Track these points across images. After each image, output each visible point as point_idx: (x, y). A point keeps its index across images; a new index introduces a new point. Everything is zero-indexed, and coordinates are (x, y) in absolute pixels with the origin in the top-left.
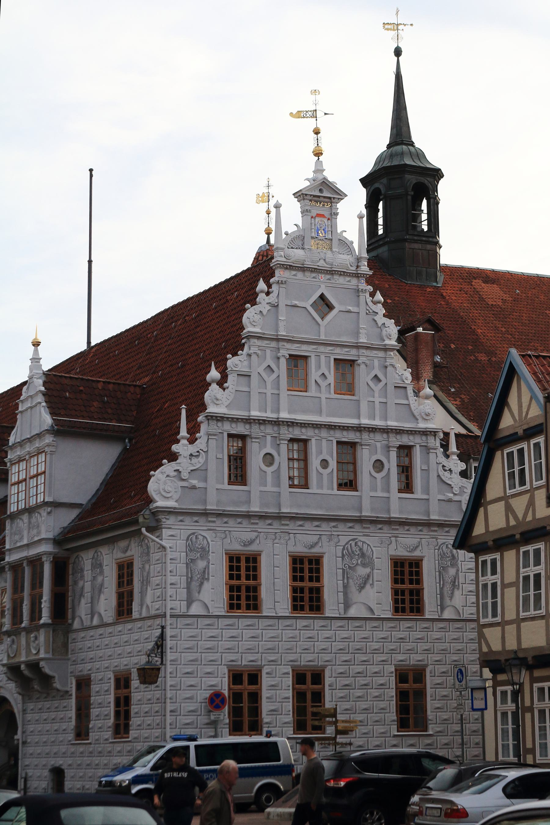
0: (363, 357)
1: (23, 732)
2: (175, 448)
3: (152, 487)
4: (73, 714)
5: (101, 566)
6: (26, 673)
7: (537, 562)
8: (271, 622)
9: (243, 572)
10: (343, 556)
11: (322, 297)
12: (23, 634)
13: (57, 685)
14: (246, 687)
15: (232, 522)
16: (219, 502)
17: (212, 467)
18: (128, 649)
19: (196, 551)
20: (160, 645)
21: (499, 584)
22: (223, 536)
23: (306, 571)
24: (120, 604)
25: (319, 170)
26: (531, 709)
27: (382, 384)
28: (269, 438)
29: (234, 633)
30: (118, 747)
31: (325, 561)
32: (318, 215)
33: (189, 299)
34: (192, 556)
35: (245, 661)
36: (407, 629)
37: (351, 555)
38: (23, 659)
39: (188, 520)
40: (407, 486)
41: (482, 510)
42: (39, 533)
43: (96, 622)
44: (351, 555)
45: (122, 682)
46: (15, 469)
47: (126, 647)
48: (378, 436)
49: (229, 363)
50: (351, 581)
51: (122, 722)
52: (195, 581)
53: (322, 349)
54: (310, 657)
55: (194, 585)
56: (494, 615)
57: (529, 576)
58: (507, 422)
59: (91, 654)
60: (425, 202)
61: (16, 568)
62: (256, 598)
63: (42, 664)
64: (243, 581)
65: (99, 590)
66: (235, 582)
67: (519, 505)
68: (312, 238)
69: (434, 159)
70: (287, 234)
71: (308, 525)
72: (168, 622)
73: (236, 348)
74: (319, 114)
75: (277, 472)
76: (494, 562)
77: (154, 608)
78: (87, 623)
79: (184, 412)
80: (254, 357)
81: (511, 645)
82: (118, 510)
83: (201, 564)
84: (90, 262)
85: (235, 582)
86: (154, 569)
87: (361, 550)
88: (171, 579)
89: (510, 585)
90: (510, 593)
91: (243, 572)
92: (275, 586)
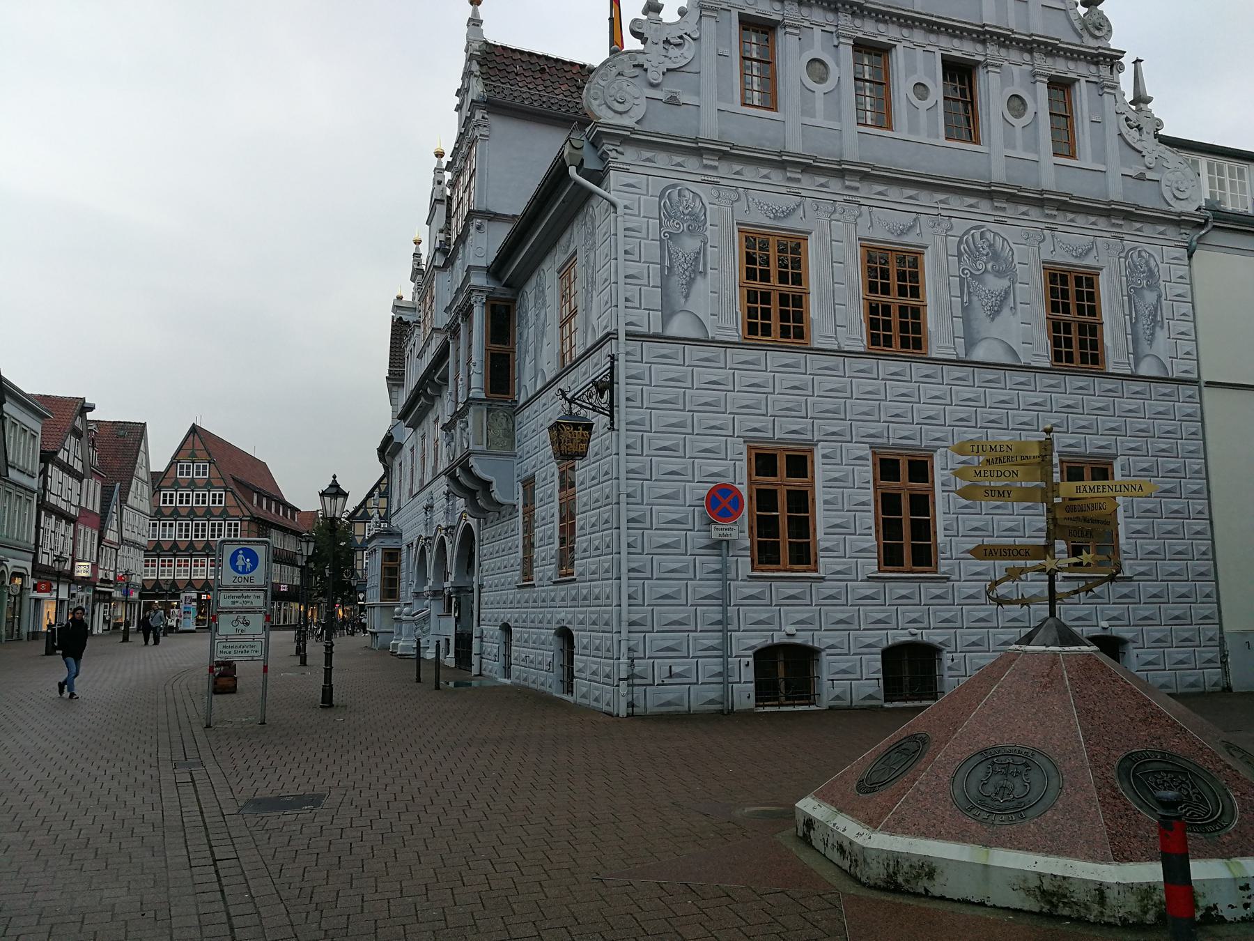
10: (960, 255)
14: (782, 482)
15: (750, 172)
29: (758, 377)
37: (974, 254)
40: (1065, 145)
44: (974, 254)
48: (1014, 55)
50: (975, 299)
55: (677, 281)
63: (472, 461)
66: (758, 285)
83: (691, 244)
92: (843, 507)
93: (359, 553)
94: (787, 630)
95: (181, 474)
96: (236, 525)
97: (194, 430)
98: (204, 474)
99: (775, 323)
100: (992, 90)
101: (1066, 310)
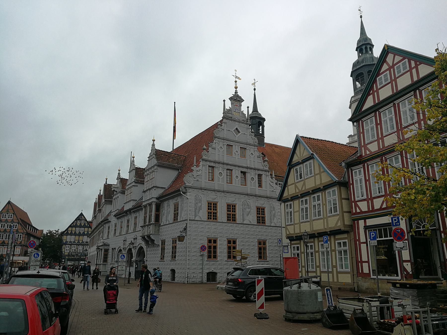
0: (248, 147)
2: (192, 168)
9: (212, 208)
11: (237, 129)
13: (156, 242)
14: (212, 244)
15: (209, 192)
20: (185, 229)
23: (231, 208)
24: (175, 217)
25: (236, 92)
29: (209, 227)
30: (173, 262)
35: (212, 236)
36: (260, 228)
40: (260, 186)
41: (286, 188)
45: (174, 242)
48: (252, 170)
56: (291, 221)
58: (296, 159)
61: (145, 206)
63: (151, 236)
66: (210, 211)
67: (300, 185)
69: (263, 116)
76: (291, 205)
81: (297, 231)
83: (200, 204)
84: (175, 127)
89: (297, 212)
91: (212, 208)
92: (222, 249)
93: (64, 246)
94: (212, 269)
95: (3, 217)
96: (21, 235)
97: (9, 203)
98: (11, 218)
99: (212, 217)
100: (248, 176)
101: (260, 214)
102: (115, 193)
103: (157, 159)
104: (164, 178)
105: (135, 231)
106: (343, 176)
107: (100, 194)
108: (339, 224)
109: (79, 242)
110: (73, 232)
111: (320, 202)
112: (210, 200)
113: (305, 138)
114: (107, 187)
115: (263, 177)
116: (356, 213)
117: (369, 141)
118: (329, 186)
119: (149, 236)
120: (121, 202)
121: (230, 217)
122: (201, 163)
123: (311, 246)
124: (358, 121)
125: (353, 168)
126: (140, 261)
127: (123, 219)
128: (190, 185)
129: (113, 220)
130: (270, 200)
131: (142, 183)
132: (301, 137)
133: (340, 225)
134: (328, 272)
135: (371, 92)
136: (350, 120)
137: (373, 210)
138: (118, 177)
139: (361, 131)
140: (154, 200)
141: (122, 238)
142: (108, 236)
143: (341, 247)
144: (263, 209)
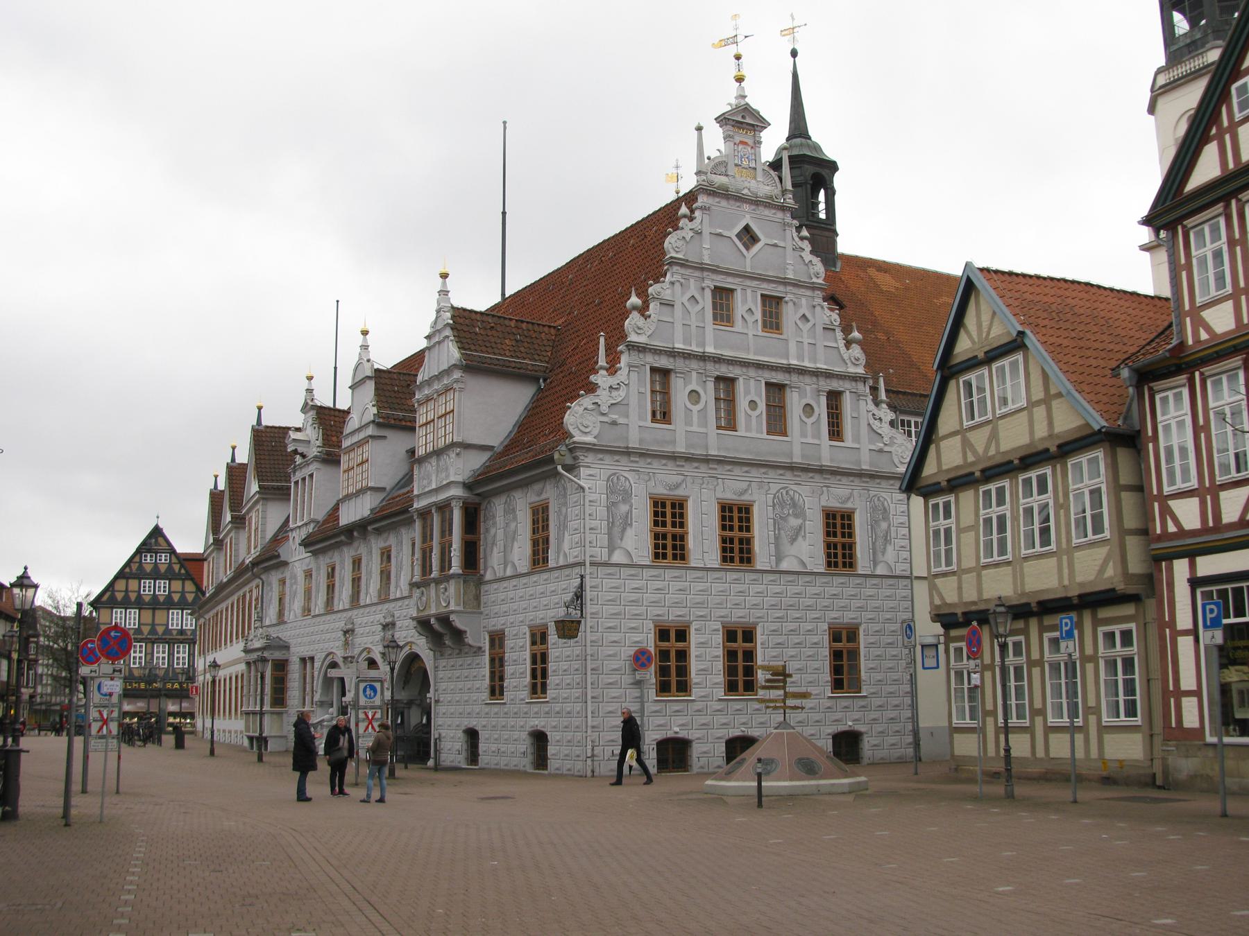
0: (789, 294)
1: (436, 690)
2: (593, 378)
3: (569, 419)
4: (486, 671)
5: (514, 511)
6: (437, 626)
7: (1001, 502)
8: (699, 574)
9: (669, 519)
10: (774, 506)
11: (747, 229)
12: (433, 585)
13: (470, 639)
14: (673, 645)
15: (656, 463)
16: (641, 441)
17: (634, 401)
18: (545, 601)
19: (617, 493)
20: (579, 596)
21: (954, 529)
22: (647, 478)
23: (735, 518)
24: (535, 553)
26: (1094, 659)
27: (810, 325)
28: (694, 374)
29: (659, 584)
30: (535, 708)
31: (756, 511)
32: (742, 142)
33: (604, 241)
34: (614, 498)
35: (672, 616)
36: (837, 584)
37: (782, 504)
38: (433, 611)
39: (608, 459)
40: (836, 432)
42: (448, 476)
43: (509, 572)
45: (539, 637)
46: (423, 410)
47: (544, 600)
48: (807, 379)
49: (650, 290)
51: (539, 680)
52: (617, 526)
53: (748, 283)
54: (741, 613)
55: (616, 530)
56: (948, 563)
57: (990, 519)
58: (964, 347)
59: (504, 608)
60: (822, 193)
61: (425, 514)
62: (683, 548)
63: (452, 617)
64: (669, 528)
65: (511, 537)
66: (660, 529)
67: (979, 439)
68: (736, 165)
69: (830, 153)
70: (709, 158)
71: (738, 471)
72: (588, 571)
73: (658, 277)
74: (739, 38)
75: (703, 412)
76: (947, 506)
77: (573, 556)
78: (500, 574)
79: (602, 340)
80: (677, 285)
81: (970, 595)
82: (533, 456)
83: (624, 508)
84: (504, 213)
85: (660, 529)
86: (572, 512)
87: (792, 499)
88: (590, 523)
90: (968, 538)
91: (669, 519)
92: (706, 659)
102: (298, 459)
103: (462, 345)
104: (488, 413)
105: (384, 598)
106: (1125, 409)
107: (233, 460)
108: (1110, 572)
109: (153, 631)
110: (133, 596)
111: (1048, 497)
112: (661, 491)
113: (996, 272)
114: (269, 441)
115: (847, 402)
116: (1165, 535)
117: (1206, 299)
118: (1077, 445)
119: (444, 620)
120: (317, 494)
121: (732, 550)
122: (624, 360)
123: (1017, 645)
124: (1171, 227)
125: (1157, 385)
126: (410, 703)
127: (336, 557)
128: (588, 439)
129: (297, 556)
130: (872, 484)
131: (408, 427)
132: (982, 270)
133: (1111, 577)
134: (1072, 730)
135: (1214, 131)
136: (1147, 221)
137: (1219, 527)
138: (306, 404)
139: (1183, 261)
140: (457, 492)
141: (338, 622)
142: (281, 613)
143: (1114, 646)
144: (848, 517)
